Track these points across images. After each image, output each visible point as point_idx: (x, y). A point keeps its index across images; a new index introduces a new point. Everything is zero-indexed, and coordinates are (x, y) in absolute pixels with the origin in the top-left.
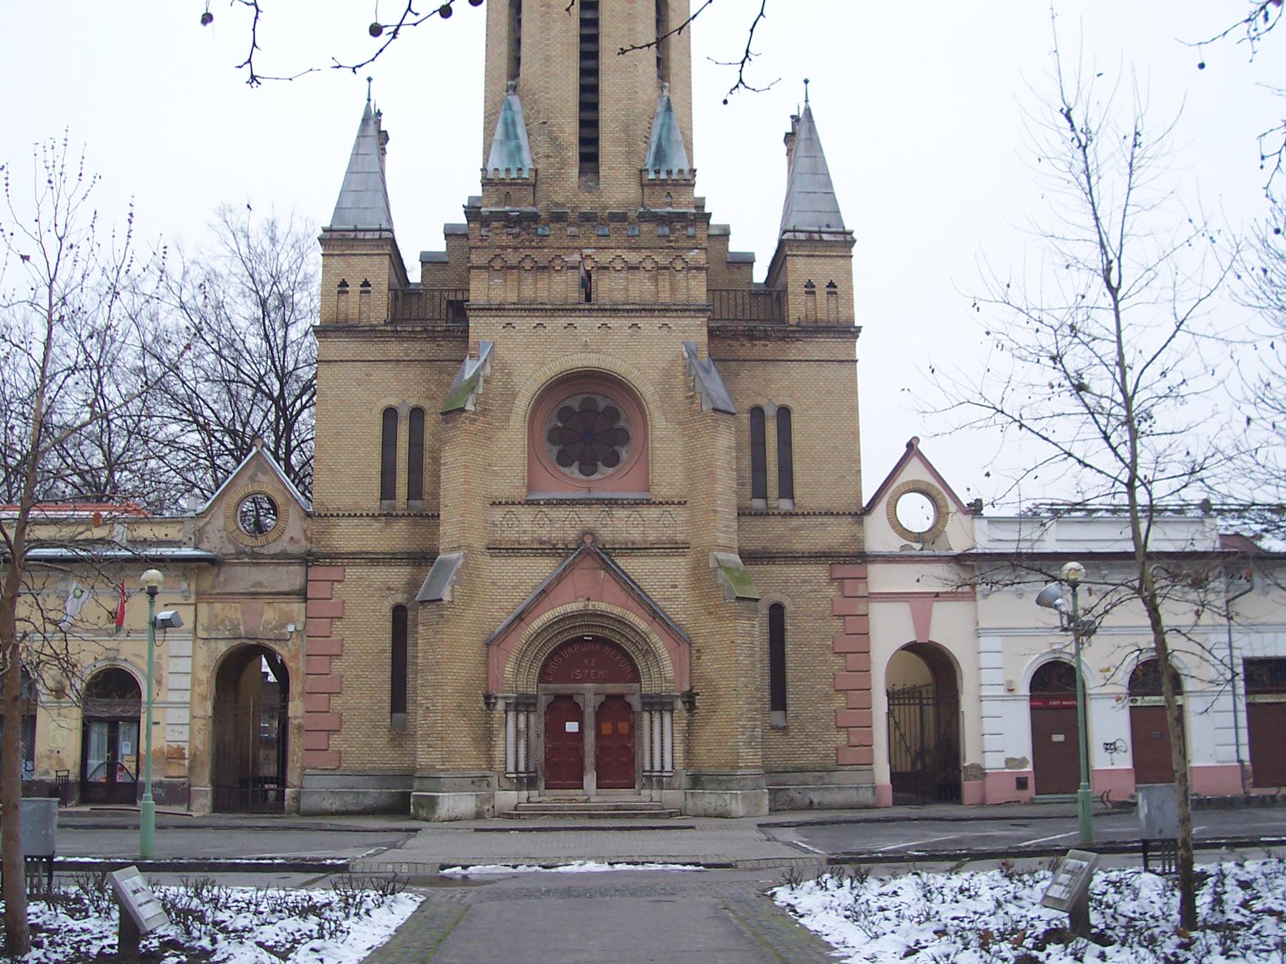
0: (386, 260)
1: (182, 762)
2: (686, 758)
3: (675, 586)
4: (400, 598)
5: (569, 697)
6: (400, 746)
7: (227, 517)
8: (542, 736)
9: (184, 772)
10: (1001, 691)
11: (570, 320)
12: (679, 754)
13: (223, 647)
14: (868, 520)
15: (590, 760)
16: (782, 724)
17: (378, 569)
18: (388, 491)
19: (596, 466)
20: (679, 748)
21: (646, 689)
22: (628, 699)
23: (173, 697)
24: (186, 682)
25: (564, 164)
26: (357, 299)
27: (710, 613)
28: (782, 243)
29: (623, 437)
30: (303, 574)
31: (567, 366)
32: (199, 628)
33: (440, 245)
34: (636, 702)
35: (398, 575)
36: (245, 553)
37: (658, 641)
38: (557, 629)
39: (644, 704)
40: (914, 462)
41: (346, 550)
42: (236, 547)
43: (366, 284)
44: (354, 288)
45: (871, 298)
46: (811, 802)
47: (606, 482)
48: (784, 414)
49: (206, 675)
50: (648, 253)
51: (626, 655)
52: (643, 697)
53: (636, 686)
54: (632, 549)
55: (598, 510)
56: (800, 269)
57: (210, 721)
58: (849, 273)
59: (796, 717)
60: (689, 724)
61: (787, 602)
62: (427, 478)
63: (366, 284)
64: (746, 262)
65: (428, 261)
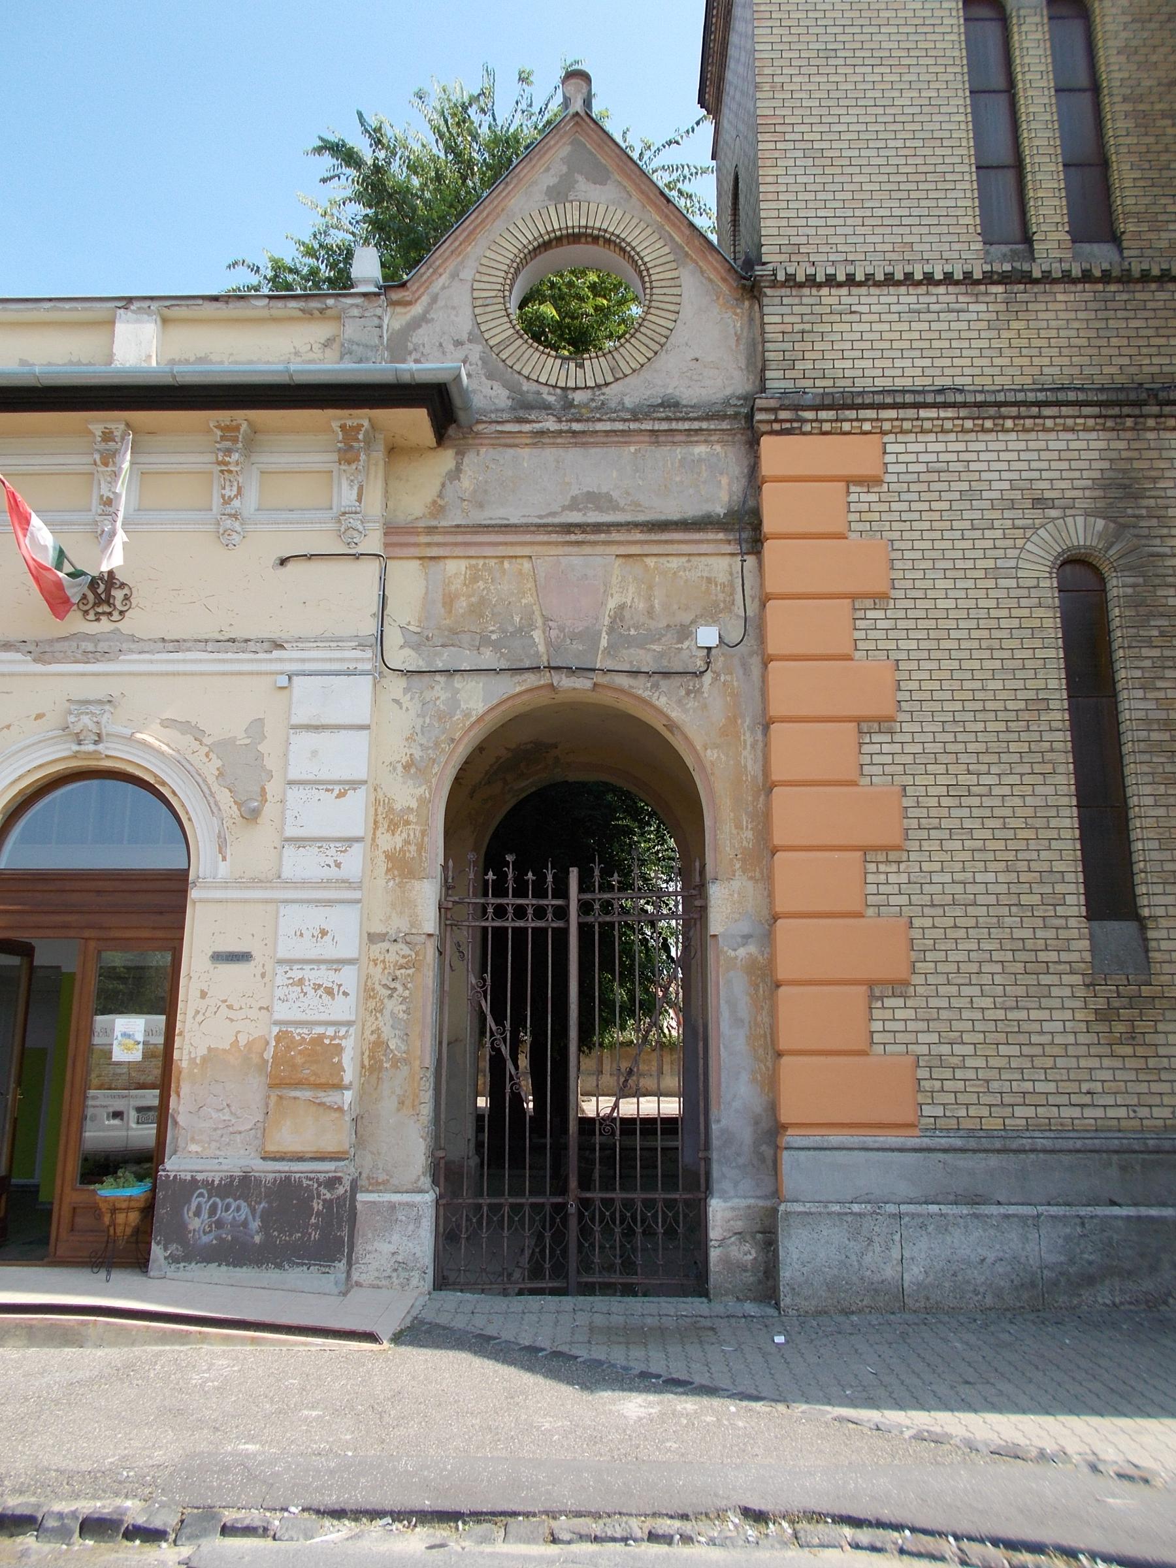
1: (331, 1098)
4: (1080, 532)
6: (1132, 1037)
9: (335, 1138)
13: (477, 702)
17: (996, 441)
23: (302, 864)
24: (351, 815)
32: (393, 638)
36: (547, 407)
42: (513, 389)
49: (424, 801)
57: (430, 954)
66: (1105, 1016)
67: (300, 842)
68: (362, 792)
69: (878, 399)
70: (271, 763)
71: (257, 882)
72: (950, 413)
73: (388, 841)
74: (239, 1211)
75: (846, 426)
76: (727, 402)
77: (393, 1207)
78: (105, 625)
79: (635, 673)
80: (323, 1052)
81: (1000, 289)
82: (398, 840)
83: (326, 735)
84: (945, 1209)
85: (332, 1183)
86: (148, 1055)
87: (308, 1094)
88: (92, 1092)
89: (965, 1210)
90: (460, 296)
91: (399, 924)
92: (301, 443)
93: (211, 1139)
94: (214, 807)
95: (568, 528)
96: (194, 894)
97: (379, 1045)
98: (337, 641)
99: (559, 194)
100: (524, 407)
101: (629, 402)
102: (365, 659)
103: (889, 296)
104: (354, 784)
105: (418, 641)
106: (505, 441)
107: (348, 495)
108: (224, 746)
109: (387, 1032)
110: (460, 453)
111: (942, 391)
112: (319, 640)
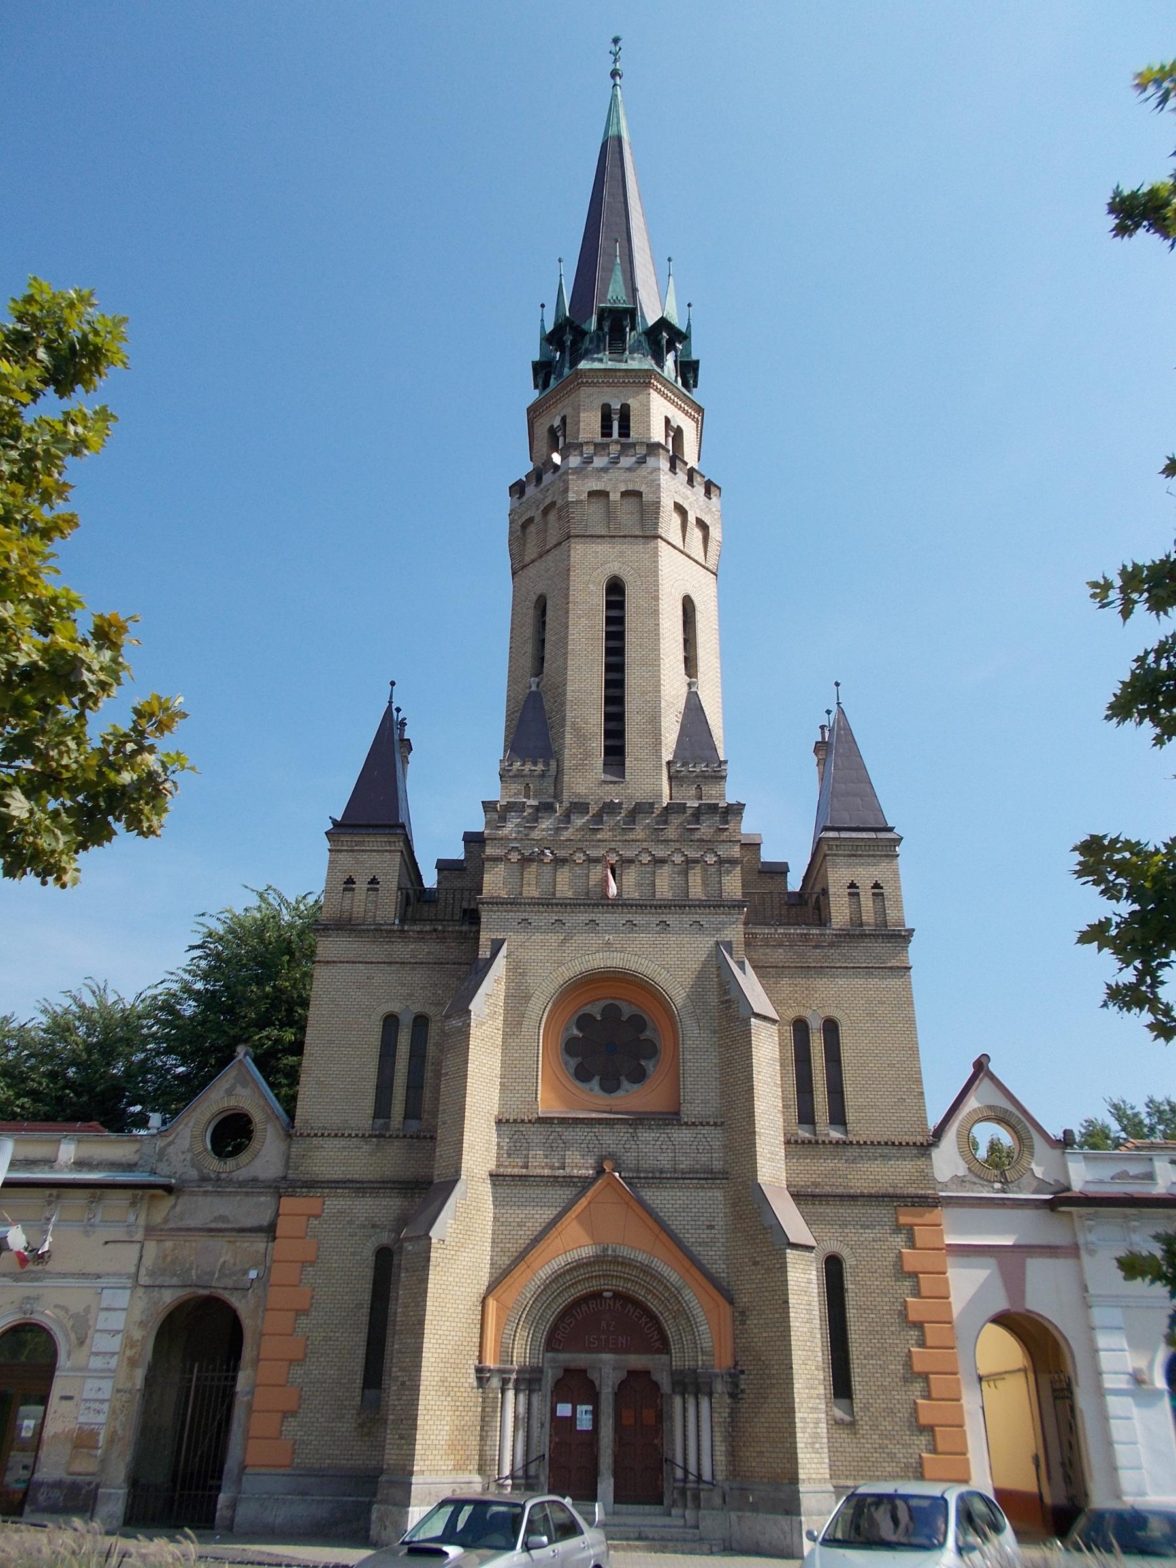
0: (397, 858)
1: (94, 1452)
2: (729, 1463)
3: (711, 1227)
4: (385, 1238)
7: (193, 1137)
8: (547, 1425)
10: (1122, 1383)
11: (592, 916)
12: (721, 1458)
13: (169, 1298)
14: (936, 1153)
15: (606, 1460)
16: (847, 1418)
18: (382, 1108)
20: (721, 1448)
21: (677, 1364)
24: (115, 1343)
25: (587, 755)
27: (756, 1263)
28: (818, 843)
29: (651, 1050)
30: (274, 1207)
31: (590, 966)
32: (143, 1271)
33: (457, 852)
34: (665, 1382)
35: (386, 1207)
37: (696, 1299)
39: (674, 1384)
40: (984, 1085)
41: (321, 1178)
42: (200, 1171)
43: (374, 881)
44: (361, 885)
45: (920, 888)
47: (634, 1098)
48: (831, 1028)
49: (145, 1338)
50: (677, 845)
51: (653, 1317)
52: (672, 1373)
53: (664, 1358)
54: (658, 1178)
56: (838, 877)
58: (896, 873)
59: (866, 1408)
60: (733, 1413)
61: (845, 1253)
62: (427, 1094)
63: (374, 881)
64: (780, 871)
65: (443, 866)
66: (361, 1426)
67: (97, 1354)
68: (120, 1336)
70: (91, 1323)
71: (80, 1369)
73: (129, 1353)
74: (57, 1494)
77: (110, 1494)
78: (40, 1267)
79: (226, 1289)
80: (94, 1434)
81: (374, 1140)
82: (134, 1351)
83: (112, 1313)
85: (89, 1484)
86: (33, 1435)
87: (85, 1450)
88: (12, 1453)
90: (187, 1133)
91: (129, 1385)
92: (118, 1202)
93: (53, 1466)
94: (68, 1340)
95: (211, 1230)
96: (57, 1373)
97: (115, 1432)
98: (120, 1275)
99: (230, 1092)
100: (204, 1179)
101: (241, 1178)
102: (129, 1283)
103: (336, 1142)
104: (118, 1332)
105: (151, 1274)
106: (193, 1194)
107: (132, 1218)
108: (75, 1316)
109: (118, 1427)
110: (178, 1197)
111: (352, 1181)
112: (115, 1275)
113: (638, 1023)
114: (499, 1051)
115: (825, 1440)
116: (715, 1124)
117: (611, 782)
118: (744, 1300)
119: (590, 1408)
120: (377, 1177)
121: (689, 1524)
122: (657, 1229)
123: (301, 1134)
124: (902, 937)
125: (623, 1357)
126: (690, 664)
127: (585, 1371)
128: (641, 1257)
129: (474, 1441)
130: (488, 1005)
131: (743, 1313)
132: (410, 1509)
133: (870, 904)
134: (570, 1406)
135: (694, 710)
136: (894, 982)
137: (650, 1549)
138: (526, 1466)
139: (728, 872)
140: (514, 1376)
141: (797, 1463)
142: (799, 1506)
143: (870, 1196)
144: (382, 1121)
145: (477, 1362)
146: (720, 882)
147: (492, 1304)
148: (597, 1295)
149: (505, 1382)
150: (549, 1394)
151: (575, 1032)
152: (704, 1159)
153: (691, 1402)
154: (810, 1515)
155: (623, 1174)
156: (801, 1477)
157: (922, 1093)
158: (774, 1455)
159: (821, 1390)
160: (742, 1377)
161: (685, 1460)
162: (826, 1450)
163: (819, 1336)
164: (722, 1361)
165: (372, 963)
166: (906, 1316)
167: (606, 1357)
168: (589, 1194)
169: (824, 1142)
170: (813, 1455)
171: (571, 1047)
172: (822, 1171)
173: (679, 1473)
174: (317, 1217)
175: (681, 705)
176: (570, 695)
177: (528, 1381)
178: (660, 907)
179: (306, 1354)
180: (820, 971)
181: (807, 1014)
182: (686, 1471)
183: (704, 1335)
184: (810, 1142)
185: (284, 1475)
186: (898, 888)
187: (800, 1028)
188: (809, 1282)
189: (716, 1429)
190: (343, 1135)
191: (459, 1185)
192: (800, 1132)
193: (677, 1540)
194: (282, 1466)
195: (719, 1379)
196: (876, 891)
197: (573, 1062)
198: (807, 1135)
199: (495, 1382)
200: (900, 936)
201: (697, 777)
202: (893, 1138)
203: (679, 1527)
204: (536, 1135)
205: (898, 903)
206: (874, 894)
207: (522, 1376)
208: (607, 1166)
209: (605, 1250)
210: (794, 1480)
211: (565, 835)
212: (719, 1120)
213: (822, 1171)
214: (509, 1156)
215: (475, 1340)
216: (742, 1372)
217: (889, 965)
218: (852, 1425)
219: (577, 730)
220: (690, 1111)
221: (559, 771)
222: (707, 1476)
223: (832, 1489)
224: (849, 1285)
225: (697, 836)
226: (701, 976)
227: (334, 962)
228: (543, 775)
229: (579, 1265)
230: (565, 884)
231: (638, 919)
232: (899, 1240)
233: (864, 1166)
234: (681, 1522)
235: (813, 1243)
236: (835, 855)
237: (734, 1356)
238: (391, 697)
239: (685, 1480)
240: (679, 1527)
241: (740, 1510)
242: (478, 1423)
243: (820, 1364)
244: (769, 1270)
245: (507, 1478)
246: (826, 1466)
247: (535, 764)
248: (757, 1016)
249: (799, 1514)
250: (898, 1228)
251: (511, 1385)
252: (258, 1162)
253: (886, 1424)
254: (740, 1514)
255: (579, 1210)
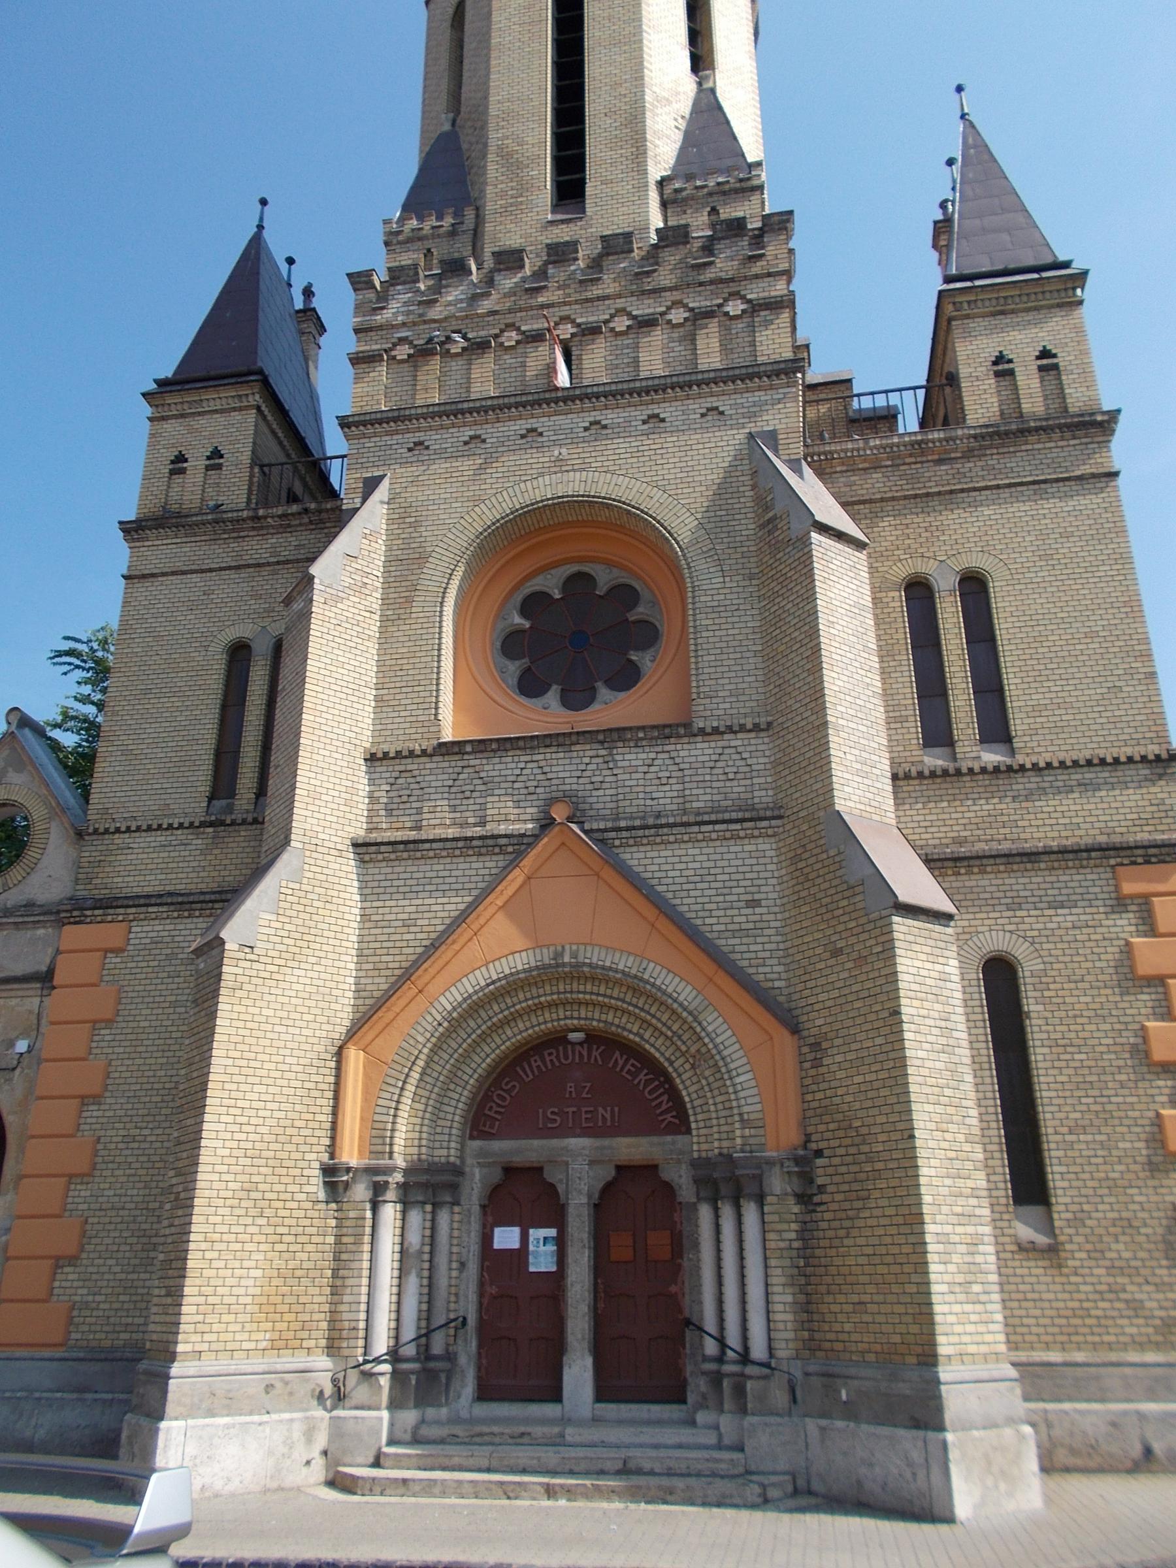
2: (801, 1325)
3: (753, 903)
5: (536, 1171)
8: (473, 1268)
11: (532, 423)
12: (784, 1316)
16: (1042, 1240)
17: (190, 923)
19: (593, 690)
20: (783, 1298)
22: (667, 1174)
25: (523, 188)
26: (200, 478)
34: (682, 1179)
37: (728, 1031)
38: (497, 1012)
41: (127, 892)
43: (216, 454)
44: (196, 463)
46: (1148, 1452)
48: (974, 587)
50: (676, 295)
54: (654, 828)
55: (586, 753)
58: (1079, 331)
59: (1077, 1221)
60: (806, 1233)
61: (1020, 951)
63: (216, 454)
64: (887, 418)
69: (125, 902)
72: (165, 908)
75: (109, 918)
76: (60, 903)
81: (211, 830)
84: (65, 1395)
89: (75, 1396)
111: (170, 894)
113: (626, 595)
114: (373, 648)
115: (994, 1278)
116: (756, 728)
117: (563, 221)
118: (816, 1023)
119: (552, 1232)
120: (214, 886)
121: (726, 1441)
122: (650, 912)
123: (96, 831)
124: (1098, 426)
125: (606, 1142)
126: (701, 58)
127: (540, 1170)
128: (625, 963)
129: (318, 1297)
130: (349, 577)
131: (816, 1046)
132: (163, 1425)
133: (1035, 383)
134: (516, 1230)
135: (708, 116)
136: (1087, 502)
137: (635, 1495)
138: (425, 1336)
139: (767, 323)
140: (398, 1177)
141: (932, 1323)
142: (939, 1409)
143: (1063, 851)
144: (224, 802)
145: (325, 1157)
146: (753, 344)
147: (355, 1058)
148: (556, 1040)
149: (378, 1190)
150: (476, 1209)
151: (518, 620)
152: (737, 788)
153: (727, 1211)
154: (966, 1426)
155: (587, 826)
156: (942, 1350)
157: (1152, 675)
158: (885, 1309)
159: (980, 1180)
160: (819, 1162)
161: (721, 1320)
162: (996, 1297)
163: (969, 1078)
164: (782, 1136)
165: (211, 570)
166: (1147, 1054)
167: (574, 1143)
168: (528, 862)
169: (971, 770)
170: (968, 1308)
171: (511, 645)
172: (968, 819)
173: (711, 1347)
174: (117, 951)
175: (684, 106)
176: (493, 110)
177: (428, 1186)
178: (648, 393)
179: (94, 1166)
180: (949, 497)
181: (928, 568)
182: (721, 1341)
183: (746, 1093)
184: (945, 773)
185: (51, 1360)
186: (1085, 353)
187: (919, 592)
188: (944, 978)
189: (773, 1262)
190: (160, 826)
191: (285, 857)
192: (926, 759)
193: (698, 1475)
194: (21, 1345)
195: (777, 1170)
196: (1045, 362)
197: (513, 668)
198: (940, 762)
199: (361, 1191)
200: (1095, 424)
201: (710, 194)
202: (1101, 753)
203: (706, 1447)
204: (436, 773)
205: (1087, 376)
206: (1041, 369)
207: (413, 1179)
208: (559, 813)
209: (558, 955)
210: (929, 1358)
211: (486, 305)
212: (763, 720)
213: (968, 819)
214: (389, 812)
215: (323, 1118)
216: (819, 1153)
217: (1078, 473)
218: (1052, 1252)
219: (506, 156)
220: (707, 713)
221: (479, 219)
222: (758, 1351)
223: (1013, 1373)
224: (1031, 1004)
225: (709, 274)
226: (724, 491)
227: (153, 575)
228: (453, 233)
229: (511, 986)
230: (484, 379)
231: (609, 417)
232: (1124, 925)
233: (1048, 804)
234: (711, 1439)
235: (947, 906)
236: (967, 317)
237: (804, 1121)
238: (261, 219)
239: (720, 1359)
240: (706, 1447)
241: (824, 1415)
242: (327, 1263)
243: (976, 1131)
244: (861, 960)
245: (378, 1361)
246: (999, 1327)
247: (440, 217)
248: (824, 529)
249: (941, 1428)
250: (1120, 903)
251: (391, 1195)
252: (36, 879)
253: (1120, 1249)
254: (824, 1422)
255: (510, 891)
